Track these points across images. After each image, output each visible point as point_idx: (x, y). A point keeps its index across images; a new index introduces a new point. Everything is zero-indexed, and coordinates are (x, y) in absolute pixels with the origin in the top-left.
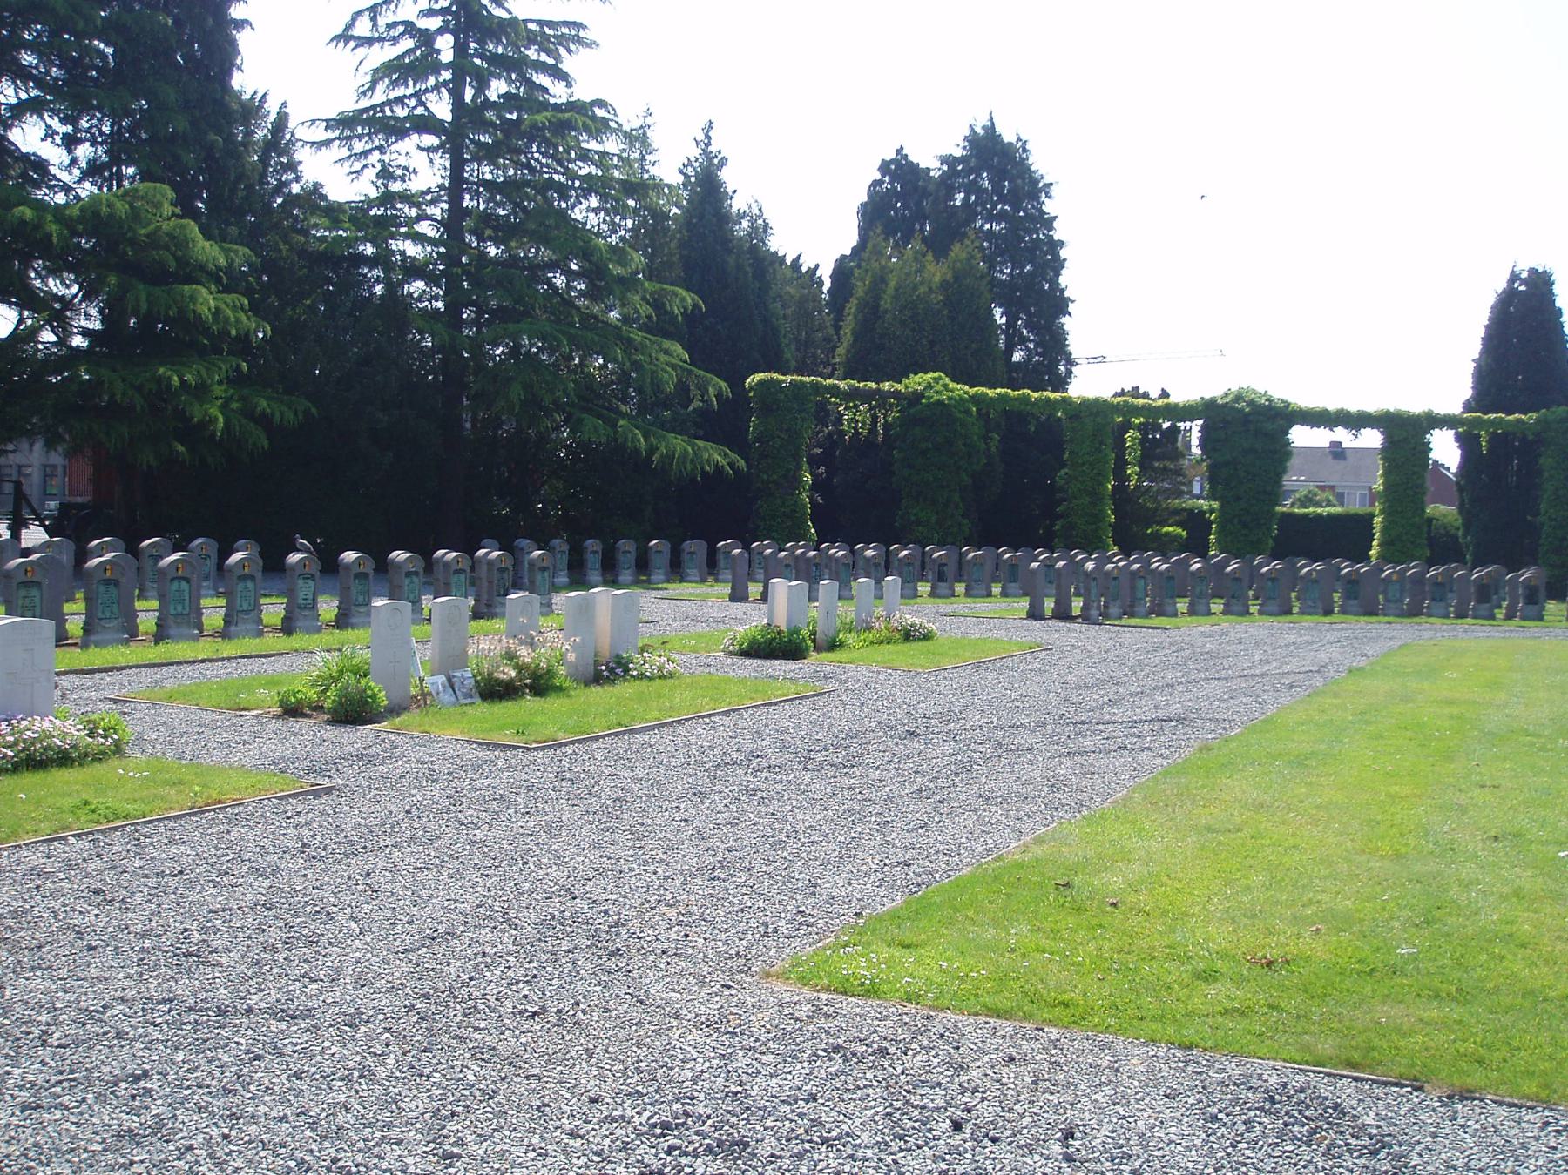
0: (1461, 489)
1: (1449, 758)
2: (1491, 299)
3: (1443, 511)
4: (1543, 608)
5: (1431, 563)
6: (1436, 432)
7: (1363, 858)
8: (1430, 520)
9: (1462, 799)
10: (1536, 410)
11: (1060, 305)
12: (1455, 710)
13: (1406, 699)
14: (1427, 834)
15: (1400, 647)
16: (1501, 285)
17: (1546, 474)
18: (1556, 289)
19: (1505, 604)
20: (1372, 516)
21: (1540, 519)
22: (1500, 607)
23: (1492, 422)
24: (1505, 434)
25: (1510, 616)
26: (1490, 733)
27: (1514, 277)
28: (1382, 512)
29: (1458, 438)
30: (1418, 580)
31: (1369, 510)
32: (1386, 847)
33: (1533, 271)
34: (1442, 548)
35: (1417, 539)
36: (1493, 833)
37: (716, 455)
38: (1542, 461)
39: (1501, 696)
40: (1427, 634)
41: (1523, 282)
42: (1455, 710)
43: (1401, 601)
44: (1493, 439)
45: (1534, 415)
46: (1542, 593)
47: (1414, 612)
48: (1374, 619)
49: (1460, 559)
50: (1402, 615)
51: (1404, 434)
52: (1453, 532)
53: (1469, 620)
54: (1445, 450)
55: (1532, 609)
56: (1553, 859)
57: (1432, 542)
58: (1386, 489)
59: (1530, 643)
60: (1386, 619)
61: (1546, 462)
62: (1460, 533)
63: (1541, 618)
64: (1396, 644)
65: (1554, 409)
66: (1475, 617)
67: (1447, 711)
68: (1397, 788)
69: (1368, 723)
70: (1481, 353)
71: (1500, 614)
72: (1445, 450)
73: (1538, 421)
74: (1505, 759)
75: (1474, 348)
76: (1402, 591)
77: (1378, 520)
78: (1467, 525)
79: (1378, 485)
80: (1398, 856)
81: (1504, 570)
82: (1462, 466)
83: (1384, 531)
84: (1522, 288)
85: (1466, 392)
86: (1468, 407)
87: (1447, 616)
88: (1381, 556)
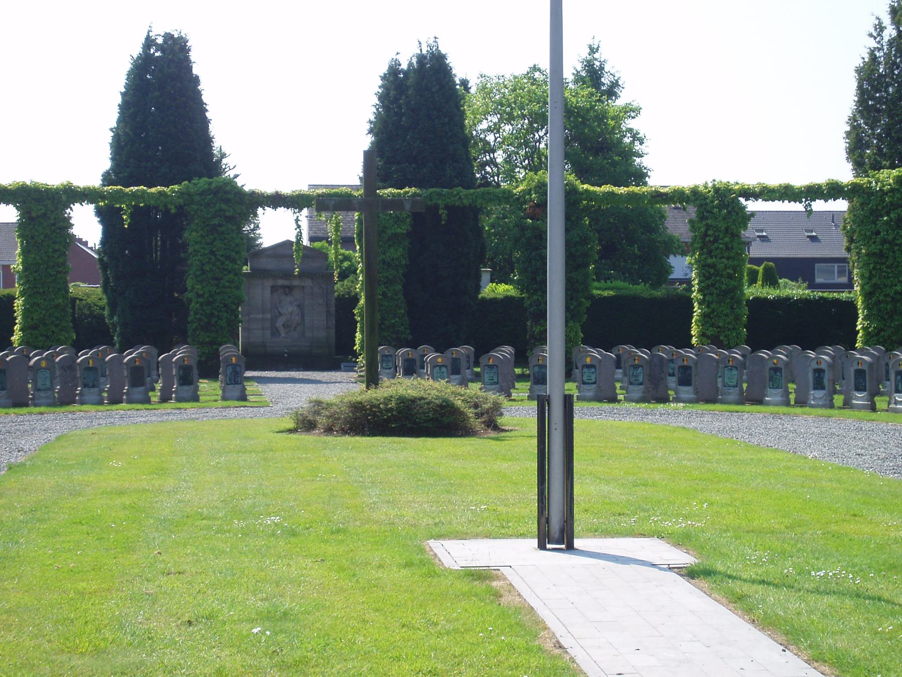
0: (104, 266)
1: (129, 548)
2: (127, 66)
3: (86, 290)
4: (197, 388)
5: (78, 346)
6: (76, 207)
7: (65, 657)
8: (74, 300)
9: (151, 588)
10: (179, 183)
11: (275, 208)
12: (126, 500)
13: (74, 493)
14: (122, 627)
15: (58, 439)
16: (137, 50)
17: (190, 250)
18: (193, 56)
19: (158, 386)
20: (12, 298)
21: (188, 295)
22: (153, 389)
23: (134, 195)
24: (148, 208)
25: (164, 399)
26: (165, 520)
27: (149, 42)
28: (23, 294)
29: (99, 212)
30: (69, 366)
31: (7, 291)
32: (85, 645)
33: (168, 37)
34: (89, 331)
35: (62, 322)
36: (187, 619)
37: (612, 293)
38: (186, 235)
39: (170, 483)
40: (83, 423)
41: (160, 48)
42: (126, 500)
43: (52, 389)
44: (137, 213)
45: (176, 187)
46: (195, 372)
47: (66, 400)
48: (24, 410)
49: (111, 343)
50: (53, 404)
51: (43, 208)
52: (97, 311)
53: (124, 405)
54: (86, 226)
55: (187, 390)
56: (248, 636)
57: (77, 323)
58: (25, 269)
59: (190, 424)
60: (37, 409)
61: (191, 236)
62: (106, 313)
63: (195, 398)
64: (53, 436)
65: (195, 181)
66: (129, 402)
67: (118, 501)
68: (84, 584)
69: (41, 520)
70: (119, 122)
71: (155, 396)
72: (86, 226)
73: (181, 194)
74: (185, 545)
75: (110, 116)
76: (52, 378)
77: (18, 304)
78: (113, 304)
79: (17, 265)
80: (98, 652)
81: (155, 351)
82: (104, 242)
83: (26, 313)
84: (158, 54)
85: (106, 164)
86: (107, 179)
87: (100, 403)
88: (23, 341)
